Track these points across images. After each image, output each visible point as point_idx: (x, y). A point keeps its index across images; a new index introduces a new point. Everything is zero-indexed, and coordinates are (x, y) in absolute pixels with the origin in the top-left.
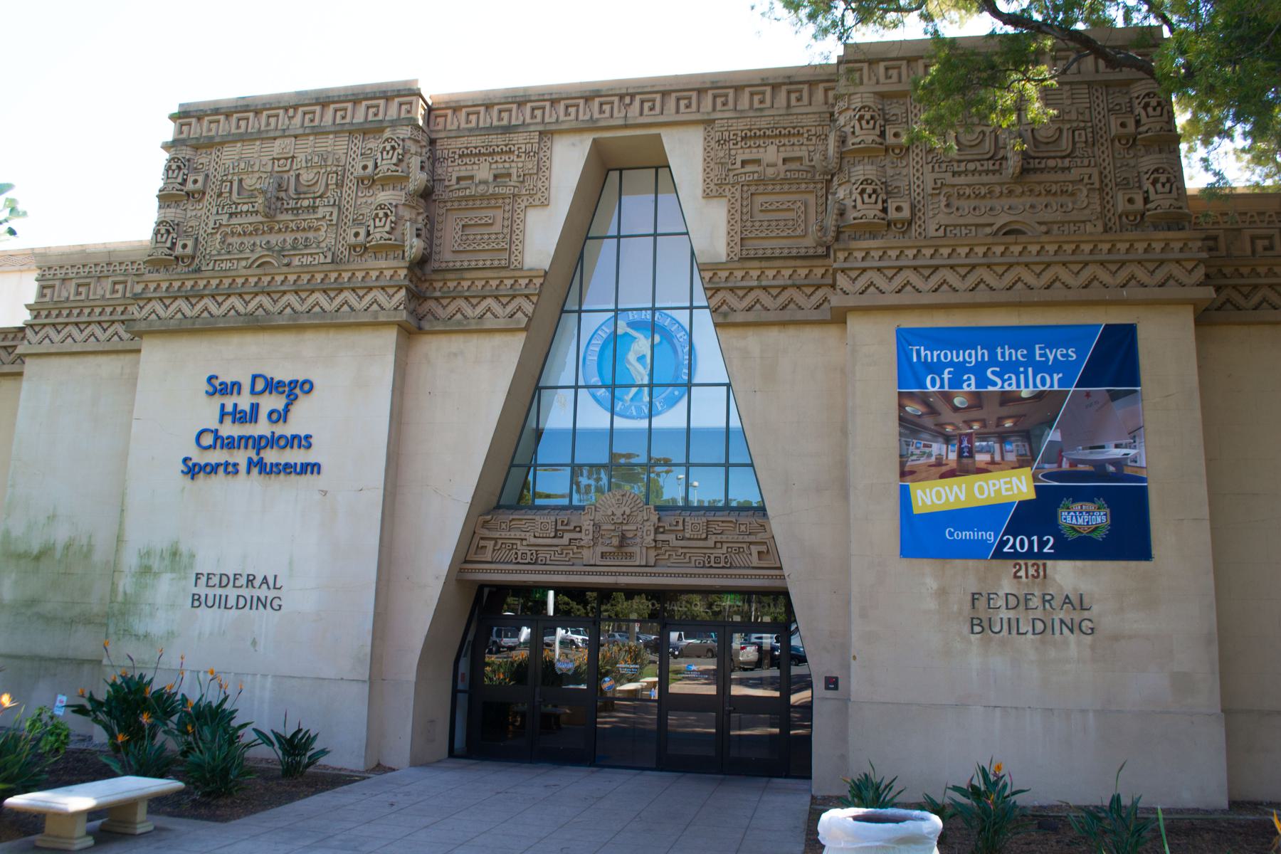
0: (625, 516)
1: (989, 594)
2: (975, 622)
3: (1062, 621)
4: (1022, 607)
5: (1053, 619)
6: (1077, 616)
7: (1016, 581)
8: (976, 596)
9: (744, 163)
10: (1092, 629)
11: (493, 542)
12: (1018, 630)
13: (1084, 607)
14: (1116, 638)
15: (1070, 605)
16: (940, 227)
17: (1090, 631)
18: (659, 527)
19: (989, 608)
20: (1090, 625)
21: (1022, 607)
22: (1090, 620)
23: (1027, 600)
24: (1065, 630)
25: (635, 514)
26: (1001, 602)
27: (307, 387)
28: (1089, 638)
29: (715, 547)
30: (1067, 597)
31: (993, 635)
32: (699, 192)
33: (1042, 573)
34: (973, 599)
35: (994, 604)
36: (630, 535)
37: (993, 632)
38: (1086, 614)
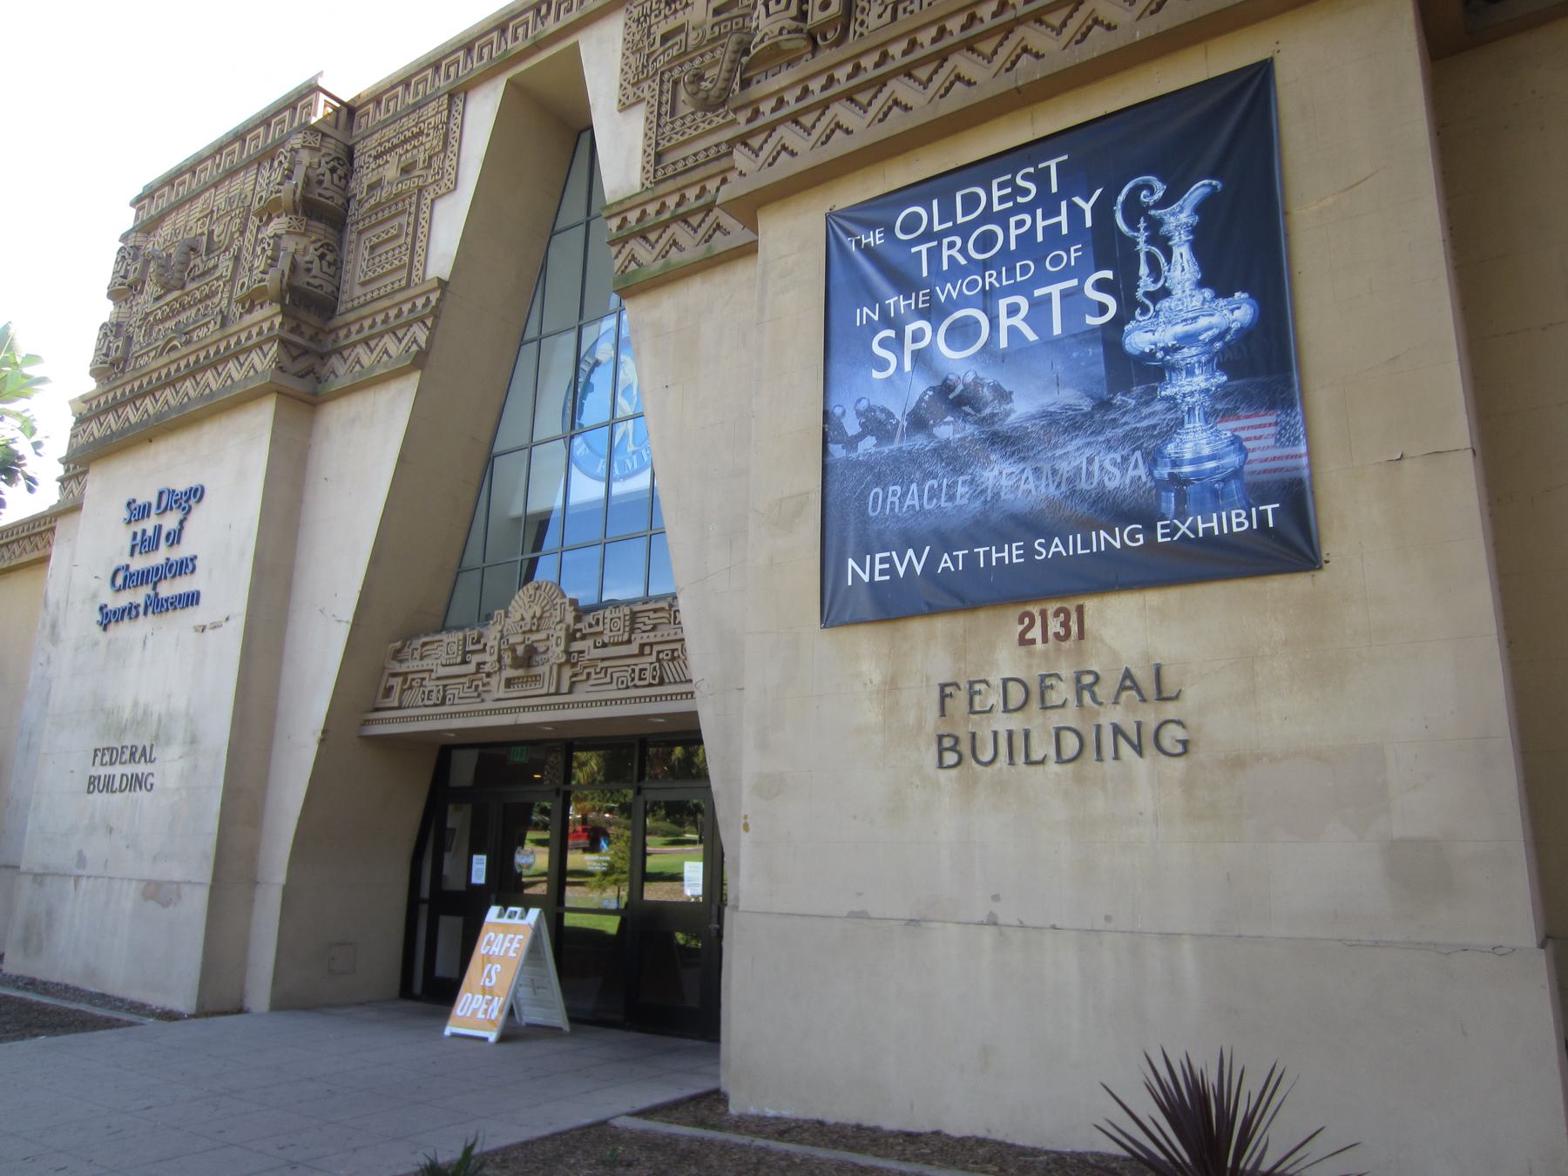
0: (535, 620)
1: (971, 684)
2: (947, 743)
3: (1117, 730)
4: (1035, 704)
5: (1099, 727)
6: (1150, 716)
7: (1023, 650)
8: (948, 690)
9: (665, 38)
10: (1185, 743)
11: (400, 679)
12: (1027, 755)
13: (1165, 695)
14: (1237, 763)
15: (1134, 693)
16: (886, 7)
17: (1179, 749)
18: (576, 631)
19: (973, 712)
20: (1178, 733)
21: (1035, 704)
22: (1179, 723)
23: (1044, 690)
24: (1125, 749)
25: (547, 614)
26: (995, 699)
27: (197, 493)
28: (1179, 764)
29: (641, 654)
30: (1128, 675)
31: (989, 769)
32: (615, 105)
33: (1074, 628)
34: (943, 697)
35: (982, 703)
36: (541, 647)
37: (978, 761)
38: (1170, 711)
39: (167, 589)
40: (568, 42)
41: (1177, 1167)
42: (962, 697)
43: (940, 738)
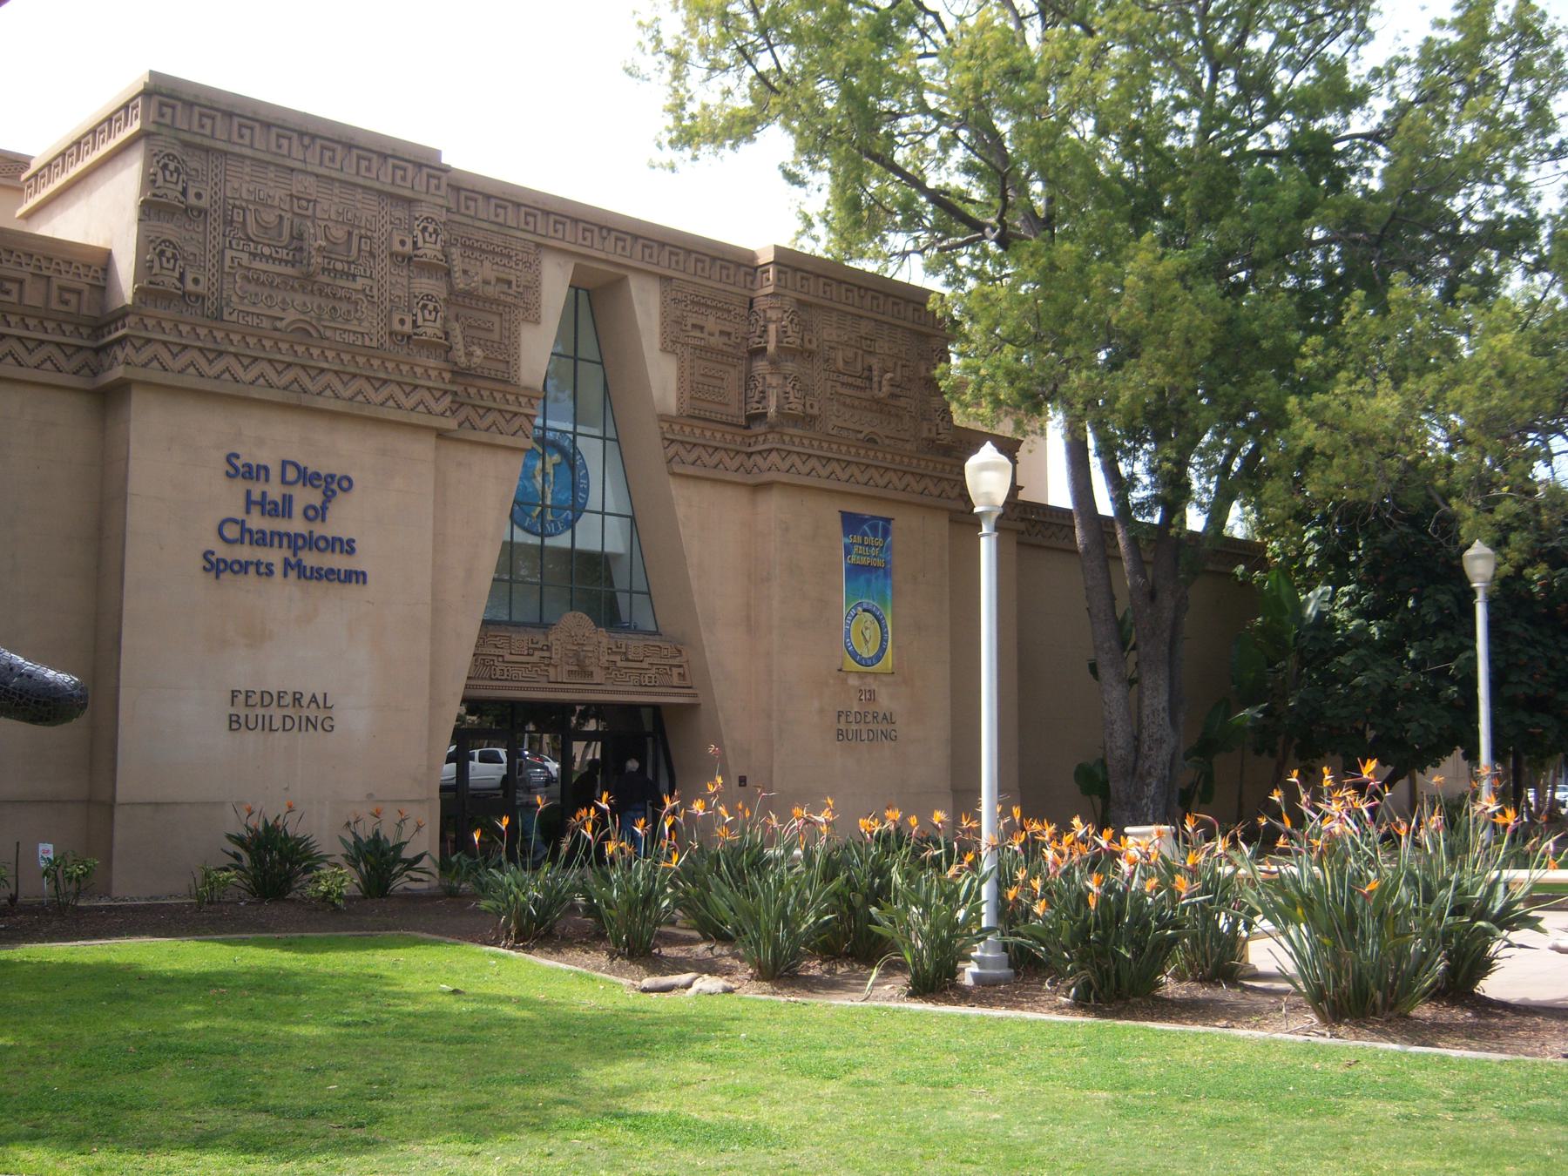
3: (308, 719)
30: (314, 696)
38: (893, 727)
39: (310, 559)
40: (623, 272)
41: (897, 837)
42: (242, 697)
43: (231, 716)
